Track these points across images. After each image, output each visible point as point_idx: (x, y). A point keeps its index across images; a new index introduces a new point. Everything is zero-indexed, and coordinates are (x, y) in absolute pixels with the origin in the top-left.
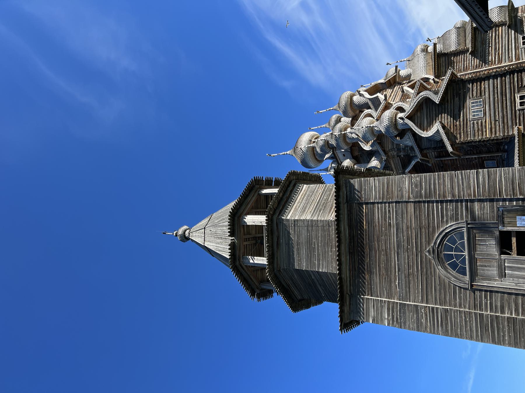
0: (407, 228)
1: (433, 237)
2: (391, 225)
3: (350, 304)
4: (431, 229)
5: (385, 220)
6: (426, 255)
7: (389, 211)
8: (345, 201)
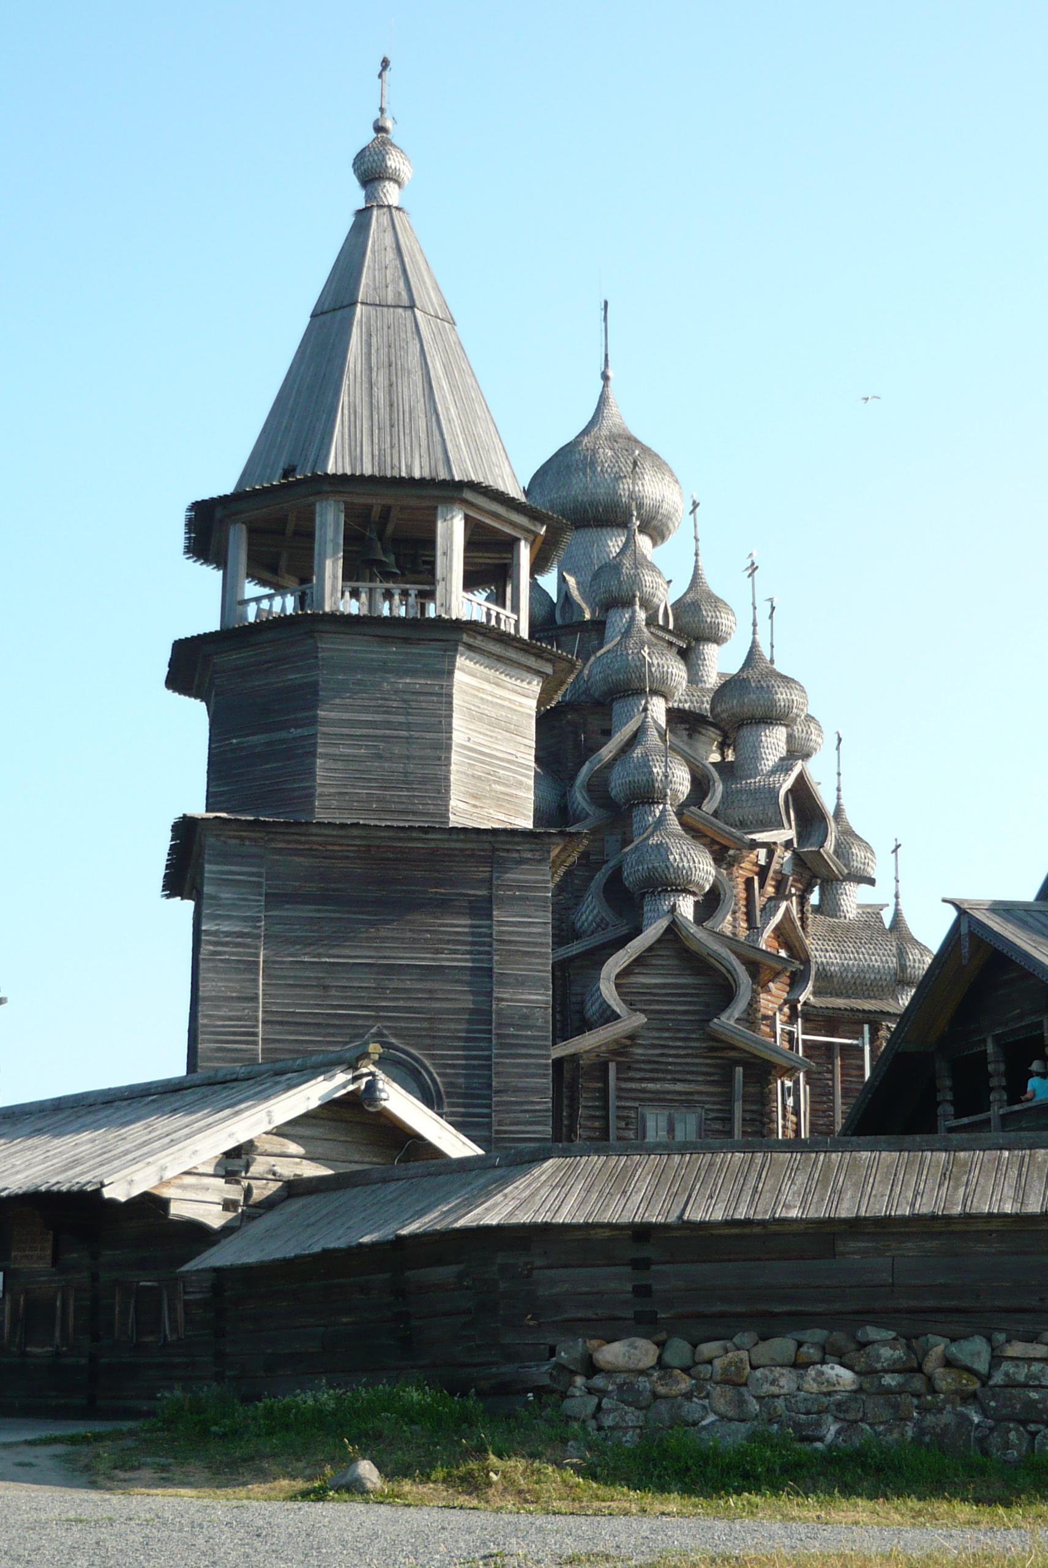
0: (430, 991)
1: (412, 1045)
2: (437, 953)
3: (242, 838)
4: (428, 1041)
5: (448, 942)
6: (372, 1027)
8: (497, 846)
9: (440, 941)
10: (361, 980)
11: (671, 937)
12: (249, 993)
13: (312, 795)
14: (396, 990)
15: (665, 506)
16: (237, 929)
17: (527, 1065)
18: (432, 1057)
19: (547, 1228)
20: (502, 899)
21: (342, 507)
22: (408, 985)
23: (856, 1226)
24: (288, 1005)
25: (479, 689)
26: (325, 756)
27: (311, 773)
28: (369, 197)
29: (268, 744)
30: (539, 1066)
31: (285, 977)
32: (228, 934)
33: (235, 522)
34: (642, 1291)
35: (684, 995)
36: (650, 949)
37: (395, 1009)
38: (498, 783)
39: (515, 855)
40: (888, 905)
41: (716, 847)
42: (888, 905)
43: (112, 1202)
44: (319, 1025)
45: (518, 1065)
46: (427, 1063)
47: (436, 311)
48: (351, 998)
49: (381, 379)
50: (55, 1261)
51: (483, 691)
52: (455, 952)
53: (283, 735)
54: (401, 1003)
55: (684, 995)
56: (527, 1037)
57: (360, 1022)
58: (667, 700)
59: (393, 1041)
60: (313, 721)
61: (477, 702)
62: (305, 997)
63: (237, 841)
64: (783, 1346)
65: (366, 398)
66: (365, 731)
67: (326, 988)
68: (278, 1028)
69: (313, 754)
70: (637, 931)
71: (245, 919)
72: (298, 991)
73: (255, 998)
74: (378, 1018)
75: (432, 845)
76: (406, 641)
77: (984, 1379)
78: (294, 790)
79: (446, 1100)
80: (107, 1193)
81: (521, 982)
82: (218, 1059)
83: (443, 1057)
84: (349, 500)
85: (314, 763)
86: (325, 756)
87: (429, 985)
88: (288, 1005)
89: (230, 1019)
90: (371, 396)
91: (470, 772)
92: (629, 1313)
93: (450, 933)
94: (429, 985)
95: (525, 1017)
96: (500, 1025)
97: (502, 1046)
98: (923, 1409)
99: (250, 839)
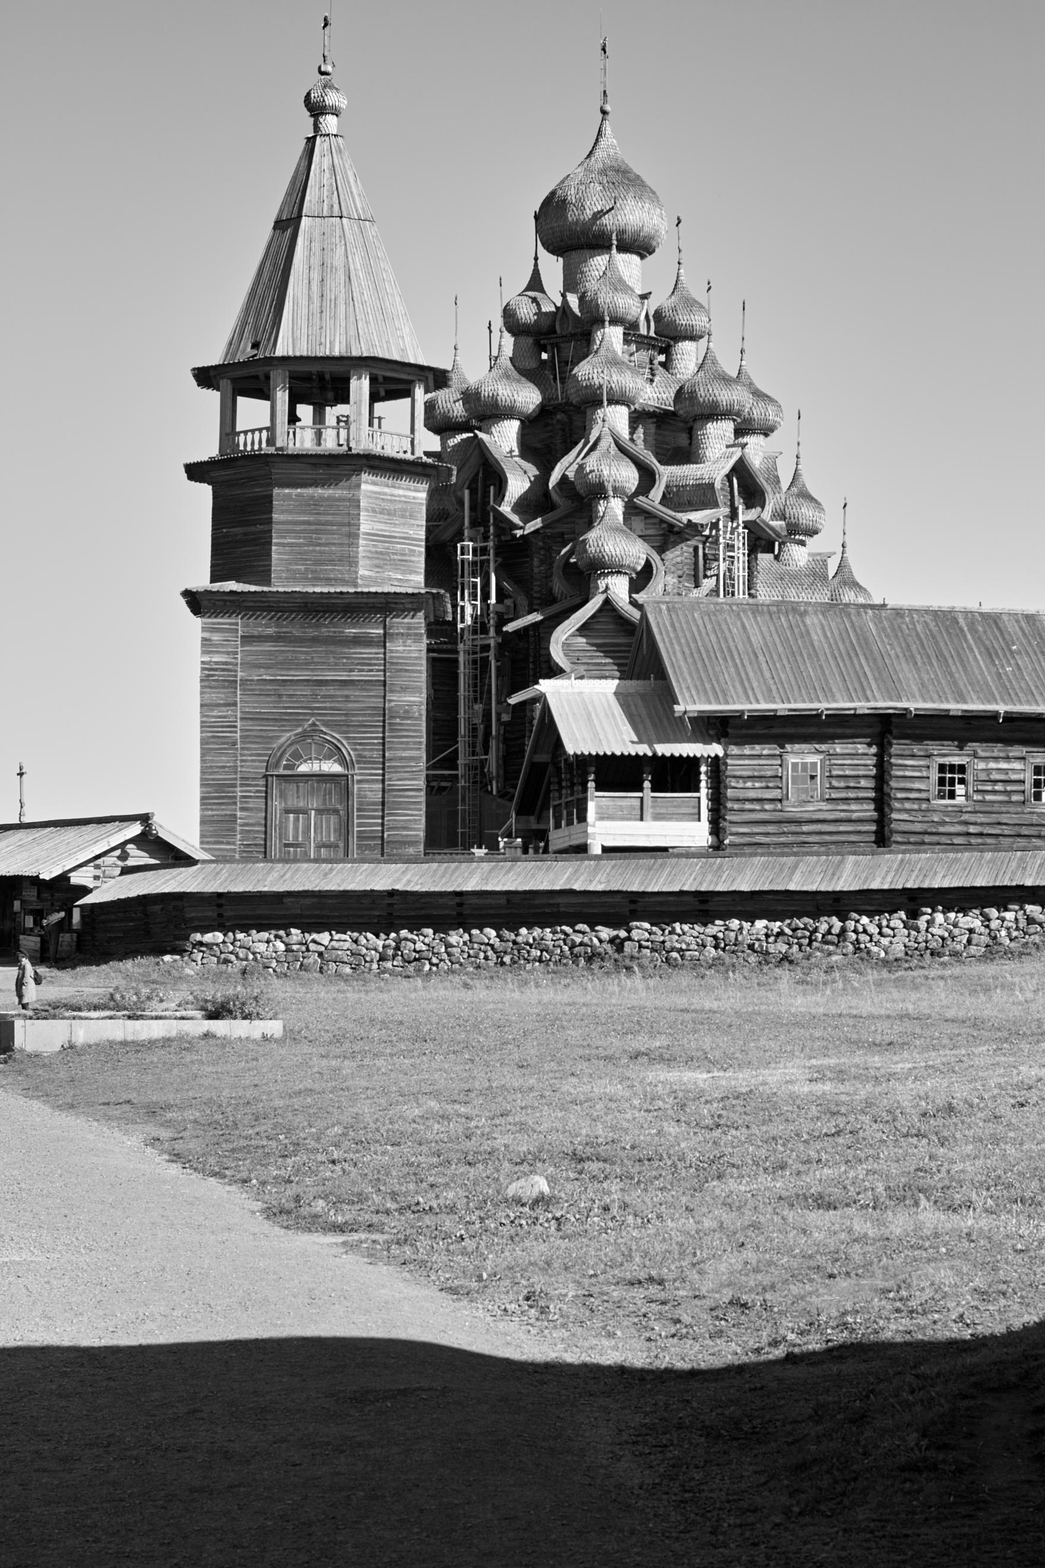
0: (347, 696)
4: (345, 729)
5: (358, 664)
7: (371, 670)
9: (353, 664)
10: (302, 690)
11: (608, 607)
12: (230, 700)
13: (270, 570)
14: (324, 696)
15: (646, 229)
16: (224, 660)
17: (407, 743)
18: (347, 738)
19: (184, 893)
20: (392, 634)
21: (287, 374)
22: (332, 692)
23: (289, 894)
24: (255, 707)
25: (380, 493)
26: (277, 544)
27: (269, 555)
28: (316, 127)
29: (245, 534)
30: (415, 743)
31: (253, 690)
32: (217, 663)
33: (223, 378)
34: (220, 915)
35: (619, 651)
36: (593, 617)
37: (325, 708)
38: (396, 554)
39: (401, 606)
40: (835, 553)
41: (664, 525)
42: (835, 553)
43: (44, 880)
44: (275, 720)
45: (402, 743)
46: (344, 742)
47: (359, 215)
48: (296, 702)
49: (316, 276)
50: (38, 897)
51: (385, 494)
52: (362, 671)
53: (252, 529)
54: (328, 705)
55: (619, 651)
56: (408, 725)
57: (301, 717)
58: (628, 406)
59: (323, 729)
60: (270, 521)
61: (379, 502)
62: (268, 702)
63: (222, 603)
64: (265, 935)
65: (306, 291)
66: (303, 527)
67: (280, 696)
68: (250, 723)
69: (270, 543)
70: (585, 601)
71: (228, 653)
72: (263, 698)
73: (235, 704)
74: (312, 715)
75: (347, 601)
76: (328, 465)
77: (326, 948)
78: (259, 566)
79: (356, 766)
80: (41, 877)
81: (404, 689)
82: (213, 743)
83: (354, 738)
84: (292, 368)
85: (271, 549)
86: (277, 544)
87: (346, 693)
88: (255, 707)
89: (220, 717)
90: (309, 288)
91: (374, 550)
92: (216, 923)
93: (359, 658)
94: (346, 693)
95: (407, 712)
96: (391, 717)
97: (392, 730)
98: (304, 958)
99: (231, 601)
